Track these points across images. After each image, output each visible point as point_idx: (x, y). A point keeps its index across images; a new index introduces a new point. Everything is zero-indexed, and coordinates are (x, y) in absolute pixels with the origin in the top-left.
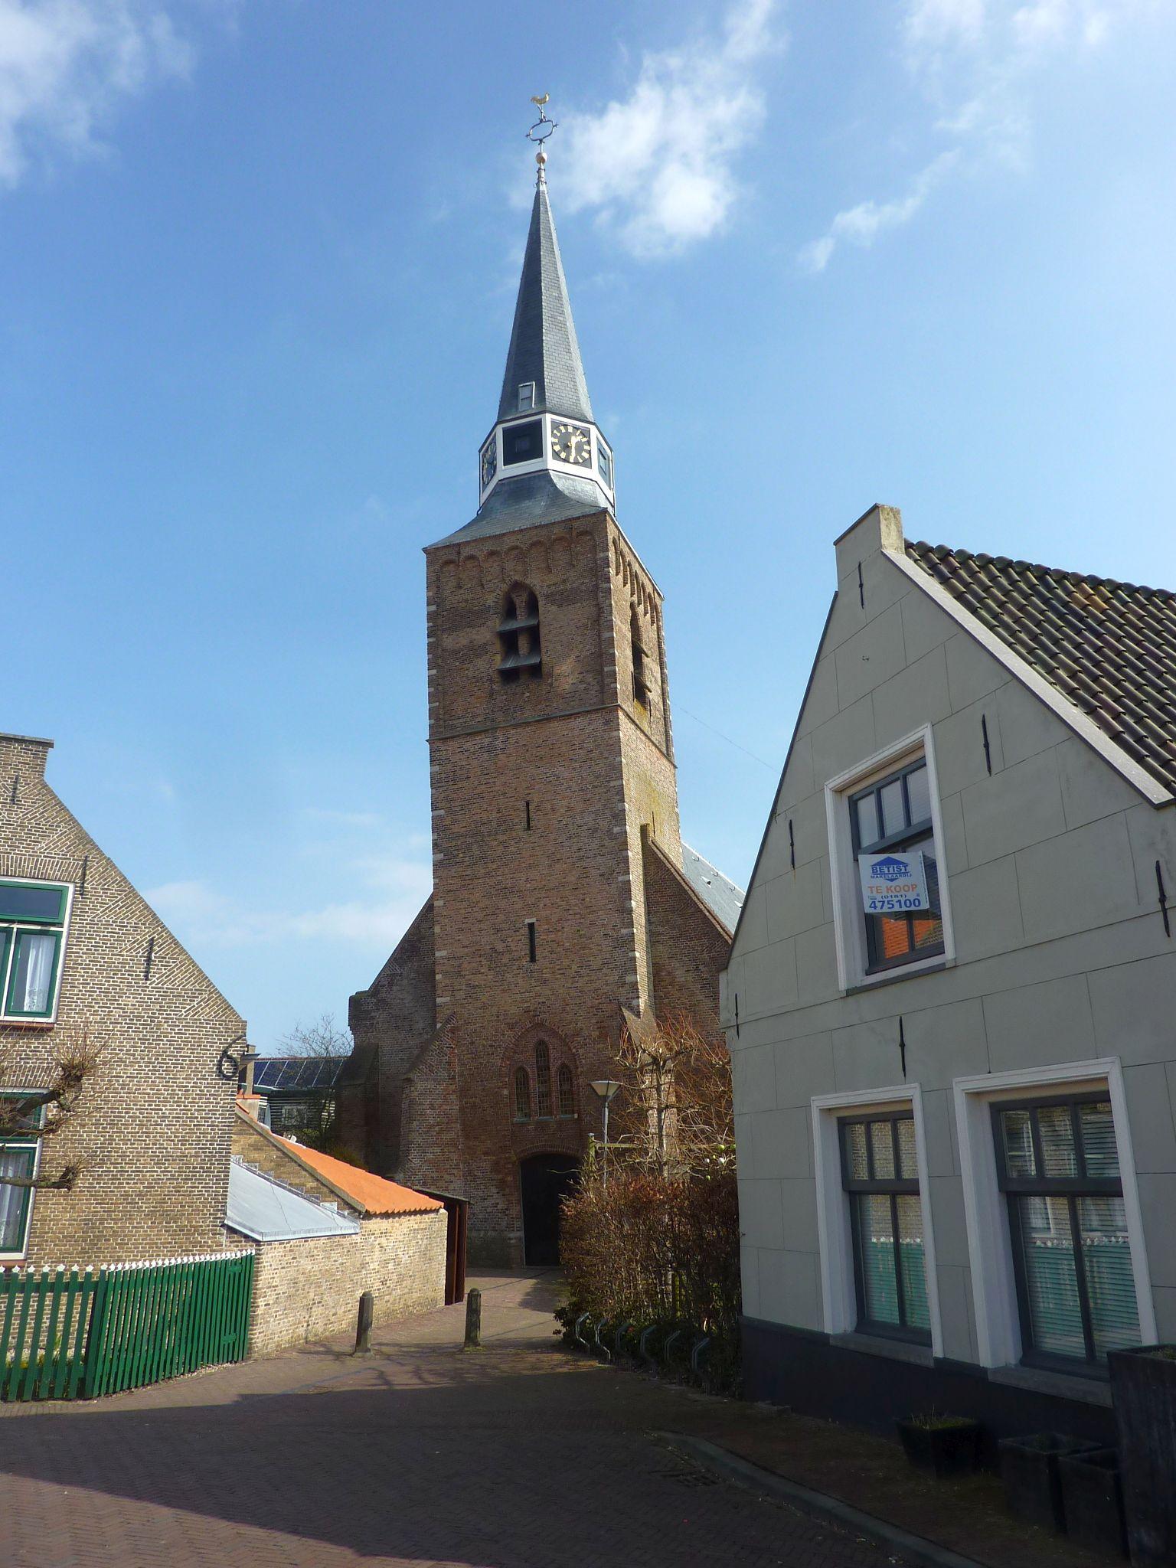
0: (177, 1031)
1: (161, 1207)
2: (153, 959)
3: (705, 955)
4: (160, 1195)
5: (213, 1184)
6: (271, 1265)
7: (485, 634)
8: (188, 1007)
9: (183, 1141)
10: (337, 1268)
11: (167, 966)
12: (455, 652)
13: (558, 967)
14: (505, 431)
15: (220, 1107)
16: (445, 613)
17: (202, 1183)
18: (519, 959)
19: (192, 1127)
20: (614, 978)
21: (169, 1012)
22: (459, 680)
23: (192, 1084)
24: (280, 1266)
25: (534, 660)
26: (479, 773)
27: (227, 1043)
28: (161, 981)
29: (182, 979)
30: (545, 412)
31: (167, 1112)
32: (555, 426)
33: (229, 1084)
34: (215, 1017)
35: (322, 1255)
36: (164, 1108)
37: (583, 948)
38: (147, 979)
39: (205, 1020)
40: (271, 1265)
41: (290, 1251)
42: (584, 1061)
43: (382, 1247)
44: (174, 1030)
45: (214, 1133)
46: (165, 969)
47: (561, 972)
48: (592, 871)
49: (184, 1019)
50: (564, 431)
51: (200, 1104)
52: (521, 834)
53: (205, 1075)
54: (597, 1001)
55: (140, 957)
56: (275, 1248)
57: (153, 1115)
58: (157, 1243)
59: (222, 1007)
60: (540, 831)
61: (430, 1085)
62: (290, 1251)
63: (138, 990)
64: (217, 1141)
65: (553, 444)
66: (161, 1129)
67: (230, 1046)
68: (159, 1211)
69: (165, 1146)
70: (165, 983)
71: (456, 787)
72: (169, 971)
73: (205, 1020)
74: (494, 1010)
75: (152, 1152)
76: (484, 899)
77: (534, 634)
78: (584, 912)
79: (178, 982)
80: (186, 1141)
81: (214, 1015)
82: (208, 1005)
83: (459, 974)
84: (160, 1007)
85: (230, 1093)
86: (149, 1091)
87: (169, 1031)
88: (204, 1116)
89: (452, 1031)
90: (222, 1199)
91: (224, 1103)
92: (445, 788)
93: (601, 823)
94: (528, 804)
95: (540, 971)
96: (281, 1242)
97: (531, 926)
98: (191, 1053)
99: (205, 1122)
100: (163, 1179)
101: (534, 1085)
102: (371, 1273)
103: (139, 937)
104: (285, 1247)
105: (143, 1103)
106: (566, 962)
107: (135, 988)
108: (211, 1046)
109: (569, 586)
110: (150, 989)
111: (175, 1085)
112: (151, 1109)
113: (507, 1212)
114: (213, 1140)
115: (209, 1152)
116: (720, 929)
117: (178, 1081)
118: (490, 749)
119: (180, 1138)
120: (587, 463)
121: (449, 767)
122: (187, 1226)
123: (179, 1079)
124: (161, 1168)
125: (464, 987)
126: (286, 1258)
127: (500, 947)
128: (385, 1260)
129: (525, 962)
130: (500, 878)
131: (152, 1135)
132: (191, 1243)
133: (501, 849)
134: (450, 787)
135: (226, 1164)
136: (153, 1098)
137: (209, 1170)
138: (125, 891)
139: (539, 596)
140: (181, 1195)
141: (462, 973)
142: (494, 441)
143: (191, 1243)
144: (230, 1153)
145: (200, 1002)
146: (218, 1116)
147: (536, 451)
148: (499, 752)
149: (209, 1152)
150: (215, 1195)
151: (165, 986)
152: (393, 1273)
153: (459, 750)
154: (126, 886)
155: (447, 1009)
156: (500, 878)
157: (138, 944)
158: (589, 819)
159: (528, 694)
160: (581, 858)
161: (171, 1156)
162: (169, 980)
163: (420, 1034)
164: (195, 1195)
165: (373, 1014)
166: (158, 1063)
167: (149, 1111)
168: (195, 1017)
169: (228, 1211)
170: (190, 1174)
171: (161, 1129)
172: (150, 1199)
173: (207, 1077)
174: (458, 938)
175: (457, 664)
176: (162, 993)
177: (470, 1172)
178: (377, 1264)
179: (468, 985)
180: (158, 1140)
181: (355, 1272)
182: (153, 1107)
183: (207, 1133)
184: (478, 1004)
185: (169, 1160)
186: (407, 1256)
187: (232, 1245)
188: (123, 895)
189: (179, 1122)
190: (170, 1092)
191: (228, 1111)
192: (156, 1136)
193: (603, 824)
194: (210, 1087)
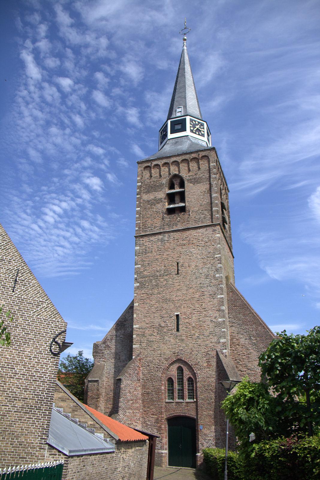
0: (27, 323)
1: (10, 429)
2: (17, 280)
3: (254, 332)
4: (9, 421)
5: (42, 417)
6: (72, 470)
7: (162, 194)
8: (35, 310)
9: (26, 389)
10: (104, 471)
11: (25, 285)
12: (148, 201)
13: (189, 334)
14: (171, 122)
15: (49, 371)
16: (145, 186)
17: (35, 416)
18: (172, 330)
19: (32, 381)
20: (215, 340)
21: (23, 312)
22: (149, 212)
23: (33, 356)
24: (77, 471)
25: (182, 204)
26: (157, 250)
27: (55, 334)
28: (21, 294)
29: (32, 294)
30: (187, 115)
31: (18, 371)
32: (191, 121)
33: (55, 358)
34: (49, 318)
35: (98, 463)
36: (16, 368)
37: (201, 326)
38: (13, 292)
39: (44, 319)
40: (72, 470)
41: (83, 461)
42: (199, 376)
43: (123, 459)
44: (26, 322)
45: (44, 387)
46: (23, 287)
47: (191, 336)
48: (206, 293)
49: (32, 317)
50: (194, 123)
51: (37, 368)
52: (175, 276)
53: (41, 351)
54: (207, 350)
55: (10, 278)
56: (75, 460)
57: (9, 371)
58: (4, 452)
59: (54, 313)
60: (183, 275)
61: (129, 382)
62: (83, 461)
63: (7, 297)
64: (45, 391)
65: (190, 127)
66: (13, 380)
67: (57, 336)
68: (8, 431)
69: (15, 391)
70: (23, 295)
71: (146, 256)
72: (25, 288)
73: (44, 319)
74: (159, 352)
75: (7, 394)
76: (156, 303)
77: (182, 196)
78: (202, 310)
79: (30, 295)
80: (27, 389)
81: (49, 317)
82: (46, 311)
83: (143, 335)
84: (19, 308)
85: (55, 363)
86: (8, 357)
87: (23, 323)
88: (39, 375)
89: (140, 360)
90: (46, 427)
91: (51, 369)
92: (141, 256)
93: (210, 272)
94: (178, 264)
95: (181, 336)
96: (78, 456)
97: (177, 316)
98: (34, 337)
99: (39, 379)
100: (12, 411)
101: (176, 386)
102: (118, 474)
103: (10, 267)
104: (80, 459)
105: (4, 363)
106: (193, 332)
107: (6, 295)
108: (46, 335)
109: (198, 176)
110: (14, 297)
111: (24, 355)
112: (8, 368)
113: (161, 441)
114: (43, 391)
115: (41, 398)
116: (261, 321)
117: (25, 353)
118: (162, 241)
119: (24, 387)
120: (203, 135)
121: (144, 247)
122: (24, 442)
123: (26, 351)
124: (11, 404)
125: (146, 341)
126: (80, 466)
127: (163, 325)
128: (124, 466)
129: (174, 332)
130: (164, 294)
131: (7, 383)
132: (25, 453)
133: (165, 282)
134: (143, 256)
135: (50, 406)
136: (10, 361)
137: (39, 409)
138: (6, 241)
139: (185, 180)
140: (22, 422)
141: (145, 335)
142: (167, 126)
143: (25, 453)
144: (53, 399)
145: (42, 308)
146: (47, 376)
147: (184, 129)
148: (165, 242)
149: (41, 398)
150: (42, 424)
151: (23, 297)
152: (127, 473)
153: (148, 240)
154: (7, 239)
155: (138, 350)
156: (164, 294)
157: (6, 250)
158: (205, 270)
159: (179, 219)
160: (201, 287)
161: (18, 398)
162: (25, 294)
163: (124, 361)
164: (30, 423)
165: (103, 351)
166: (15, 341)
167: (7, 369)
168: (38, 317)
169: (49, 435)
170: (29, 410)
171: (13, 380)
172: (3, 423)
173: (42, 352)
174: (143, 320)
175: (149, 206)
176: (20, 301)
177: (145, 422)
178: (121, 468)
179: (147, 340)
180: (11, 387)
181: (112, 473)
182: (10, 366)
183: (40, 386)
184: (152, 349)
185: (16, 400)
186: (133, 464)
187: (51, 456)
188: (4, 243)
189: (24, 377)
190: (20, 359)
191: (53, 374)
192: (10, 384)
193: (211, 273)
194: (44, 358)
